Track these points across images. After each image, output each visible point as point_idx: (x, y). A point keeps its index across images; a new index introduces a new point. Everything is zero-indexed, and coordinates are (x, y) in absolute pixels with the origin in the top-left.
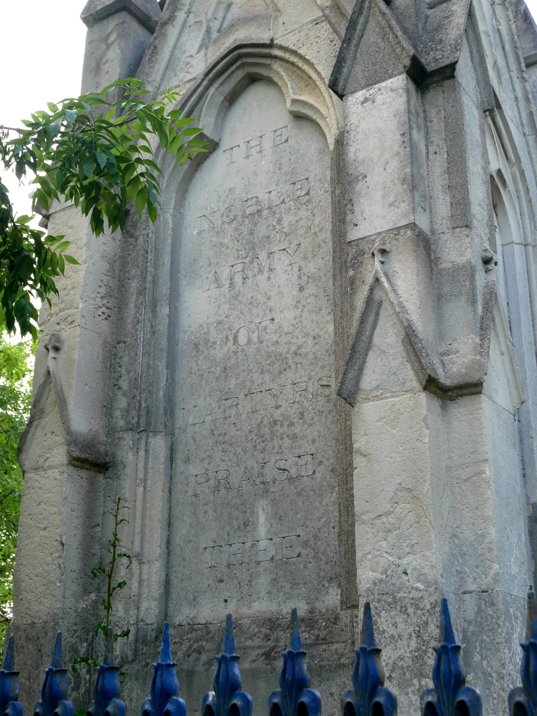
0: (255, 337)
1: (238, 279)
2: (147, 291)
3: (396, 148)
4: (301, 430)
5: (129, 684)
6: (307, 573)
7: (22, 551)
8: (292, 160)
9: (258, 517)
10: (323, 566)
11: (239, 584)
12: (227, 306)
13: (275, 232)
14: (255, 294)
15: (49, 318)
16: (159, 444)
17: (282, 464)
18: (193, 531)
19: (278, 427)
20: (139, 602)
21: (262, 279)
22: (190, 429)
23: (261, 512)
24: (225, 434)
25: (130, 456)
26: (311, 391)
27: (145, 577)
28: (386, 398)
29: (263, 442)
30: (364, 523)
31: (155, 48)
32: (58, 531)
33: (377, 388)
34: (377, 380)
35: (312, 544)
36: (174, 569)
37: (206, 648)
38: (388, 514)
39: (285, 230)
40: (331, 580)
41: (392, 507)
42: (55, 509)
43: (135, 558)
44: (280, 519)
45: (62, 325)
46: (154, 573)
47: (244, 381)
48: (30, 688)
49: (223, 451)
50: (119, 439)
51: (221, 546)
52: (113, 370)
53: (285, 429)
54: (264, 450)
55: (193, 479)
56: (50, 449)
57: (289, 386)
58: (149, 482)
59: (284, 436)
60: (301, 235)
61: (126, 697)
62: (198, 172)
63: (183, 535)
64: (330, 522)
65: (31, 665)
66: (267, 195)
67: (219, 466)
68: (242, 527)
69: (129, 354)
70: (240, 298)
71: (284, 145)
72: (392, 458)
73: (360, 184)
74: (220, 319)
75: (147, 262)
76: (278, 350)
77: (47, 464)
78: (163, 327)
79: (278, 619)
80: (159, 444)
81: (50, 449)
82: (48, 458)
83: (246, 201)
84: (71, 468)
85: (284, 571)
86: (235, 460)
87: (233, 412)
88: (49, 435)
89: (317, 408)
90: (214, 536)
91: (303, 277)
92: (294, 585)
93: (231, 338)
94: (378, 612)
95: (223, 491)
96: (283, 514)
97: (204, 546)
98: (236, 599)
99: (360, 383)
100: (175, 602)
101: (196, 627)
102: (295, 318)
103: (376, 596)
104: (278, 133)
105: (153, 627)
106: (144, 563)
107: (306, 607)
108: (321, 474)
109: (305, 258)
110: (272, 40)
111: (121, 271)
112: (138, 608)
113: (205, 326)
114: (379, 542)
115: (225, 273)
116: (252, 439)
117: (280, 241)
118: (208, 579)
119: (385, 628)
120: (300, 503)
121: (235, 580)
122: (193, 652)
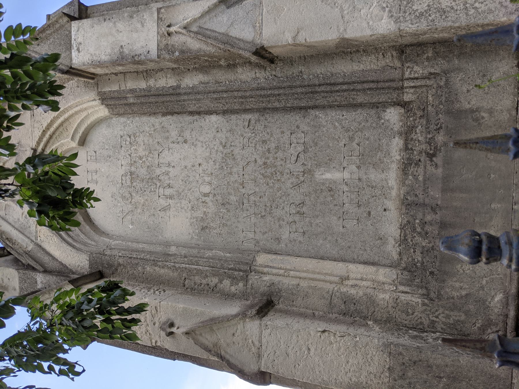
0: (207, 179)
1: (168, 192)
2: (156, 259)
3: (111, 24)
4: (274, 142)
5: (447, 290)
6: (372, 137)
7: (325, 379)
8: (108, 147)
9: (327, 180)
10: (369, 124)
11: (373, 197)
12: (183, 202)
13: (146, 161)
14: (180, 178)
15: (148, 334)
16: (262, 259)
17: (294, 158)
18: (329, 238)
19: (268, 161)
20: (377, 282)
21: (173, 172)
22: (259, 236)
23: (324, 177)
24: (266, 206)
25: (266, 278)
26: (250, 134)
27: (359, 276)
28: (262, 20)
29: (276, 174)
30: (345, 30)
31: (7, 239)
32: (312, 334)
33: (254, 27)
34: (249, 27)
35: (352, 133)
36: (356, 258)
37: (421, 217)
38: (342, 10)
39: (147, 153)
40: (379, 118)
41: (337, 7)
42: (294, 337)
43: (344, 282)
44: (330, 160)
45: (156, 320)
46: (356, 270)
47: (234, 189)
48: (449, 377)
49: (277, 208)
50: (252, 288)
51: (343, 212)
52: (202, 292)
53: (271, 155)
54: (282, 173)
55: (292, 235)
56: (246, 339)
57: (244, 152)
58: (288, 267)
59: (275, 156)
60: (153, 141)
61: (458, 294)
62: (95, 222)
63: (331, 247)
64: (339, 118)
65: (427, 375)
66: (123, 168)
67: (286, 212)
68: (332, 193)
69: (194, 276)
70: (180, 191)
71: (97, 153)
72: (303, 10)
73: (125, 50)
74: (190, 208)
75: (137, 258)
76: (220, 160)
77: (257, 343)
78: (184, 252)
79: (403, 163)
80: (262, 259)
81: (246, 339)
82: (253, 342)
83: (122, 184)
84: (264, 318)
85: (369, 158)
86: (284, 198)
87: (252, 198)
88: (235, 339)
89: (262, 130)
90: (335, 218)
91: (178, 140)
92: (379, 148)
93: (204, 199)
94: (413, 12)
95: (304, 209)
96: (328, 158)
97: (341, 228)
98: (385, 200)
99: (249, 40)
100: (381, 258)
101: (402, 238)
102: (203, 147)
103: (401, 15)
104: (89, 158)
105: (400, 274)
106: (348, 276)
107: (397, 138)
108: (305, 127)
109: (167, 138)
110: (32, 149)
111: (137, 280)
112: (383, 283)
113: (192, 220)
114: (361, 15)
115: (163, 202)
116: (273, 183)
117: (153, 158)
118: (366, 225)
119: (426, 4)
120: (322, 144)
121: (370, 200)
122: (423, 230)
